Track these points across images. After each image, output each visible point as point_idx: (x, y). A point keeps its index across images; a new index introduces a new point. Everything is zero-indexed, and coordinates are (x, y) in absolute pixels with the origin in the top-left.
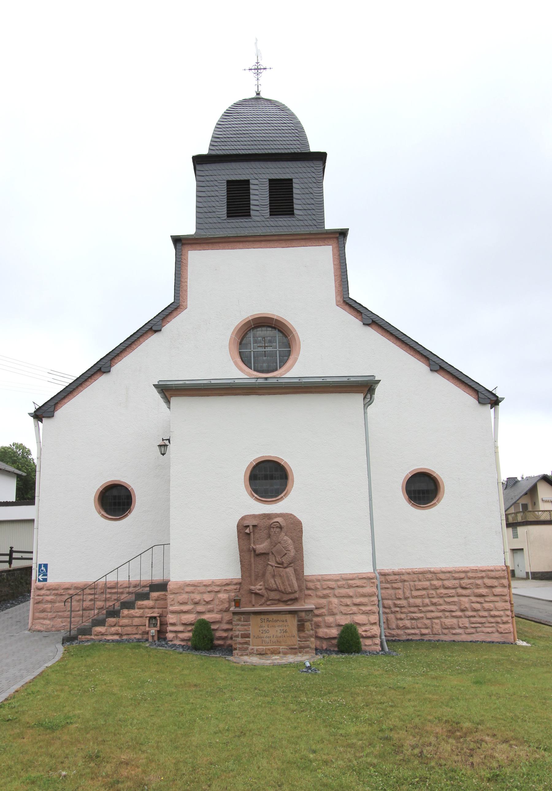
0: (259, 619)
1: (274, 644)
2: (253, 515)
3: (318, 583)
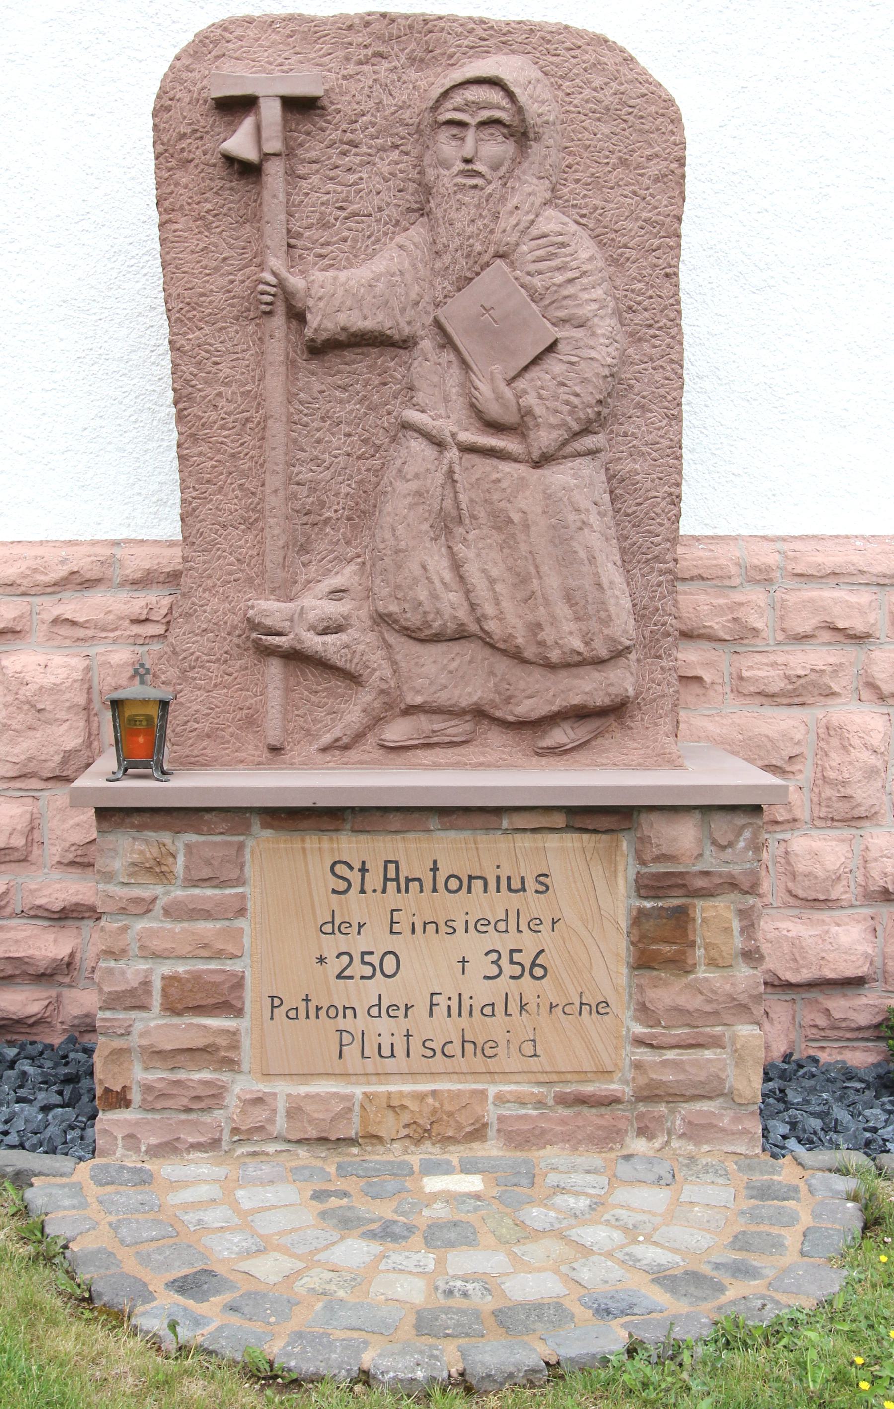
3: (757, 595)
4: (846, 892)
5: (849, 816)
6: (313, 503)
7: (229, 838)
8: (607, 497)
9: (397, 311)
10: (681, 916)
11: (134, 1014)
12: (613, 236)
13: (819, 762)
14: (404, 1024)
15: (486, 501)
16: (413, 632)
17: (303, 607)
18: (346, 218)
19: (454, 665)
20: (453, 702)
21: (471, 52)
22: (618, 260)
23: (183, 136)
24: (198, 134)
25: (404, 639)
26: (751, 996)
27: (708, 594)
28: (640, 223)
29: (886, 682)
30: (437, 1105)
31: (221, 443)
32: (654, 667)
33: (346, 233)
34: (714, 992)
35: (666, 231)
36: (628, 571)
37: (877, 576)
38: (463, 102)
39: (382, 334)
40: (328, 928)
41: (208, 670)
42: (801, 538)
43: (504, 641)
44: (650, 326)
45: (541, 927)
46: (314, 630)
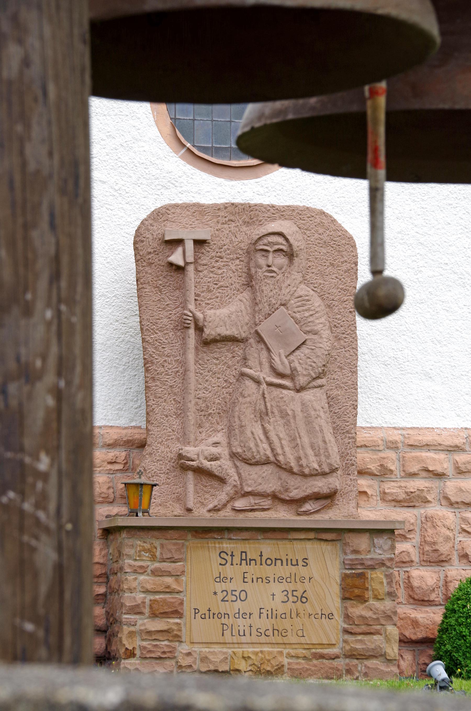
0: (214, 556)
1: (263, 639)
2: (195, 205)
3: (391, 454)
4: (438, 597)
5: (437, 560)
6: (204, 407)
7: (178, 541)
8: (327, 405)
9: (240, 327)
10: (362, 576)
11: (137, 617)
12: (328, 296)
13: (423, 534)
14: (249, 621)
15: (277, 406)
16: (248, 460)
17: (202, 450)
18: (218, 288)
19: (264, 475)
20: (264, 490)
21: (269, 219)
22: (330, 306)
23: (150, 253)
24: (157, 253)
25: (243, 464)
26: (392, 612)
27: (368, 453)
28: (339, 290)
29: (453, 496)
30: (263, 656)
31: (166, 381)
32: (347, 479)
33: (218, 294)
34: (377, 610)
35: (350, 293)
36: (336, 437)
37: (447, 446)
38: (267, 242)
39: (234, 336)
40: (218, 580)
41: (160, 477)
42: (411, 428)
43: (286, 465)
44: (344, 333)
45: (304, 581)
46: (207, 459)
